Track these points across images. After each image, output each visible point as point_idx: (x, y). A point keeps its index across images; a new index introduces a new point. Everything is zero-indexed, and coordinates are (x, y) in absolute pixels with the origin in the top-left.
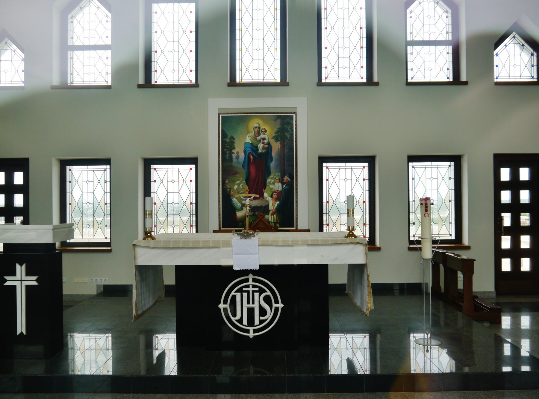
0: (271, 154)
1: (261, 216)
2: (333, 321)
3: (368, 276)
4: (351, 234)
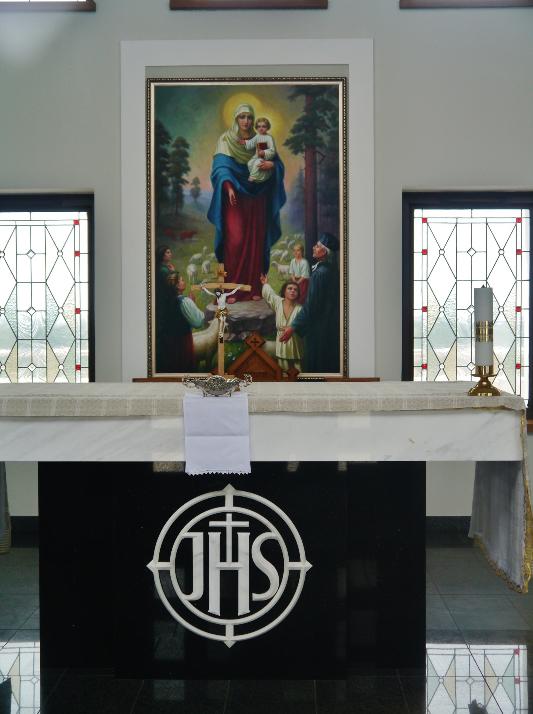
0: (282, 186)
1: (255, 342)
2: (437, 609)
3: (526, 491)
4: (484, 387)
